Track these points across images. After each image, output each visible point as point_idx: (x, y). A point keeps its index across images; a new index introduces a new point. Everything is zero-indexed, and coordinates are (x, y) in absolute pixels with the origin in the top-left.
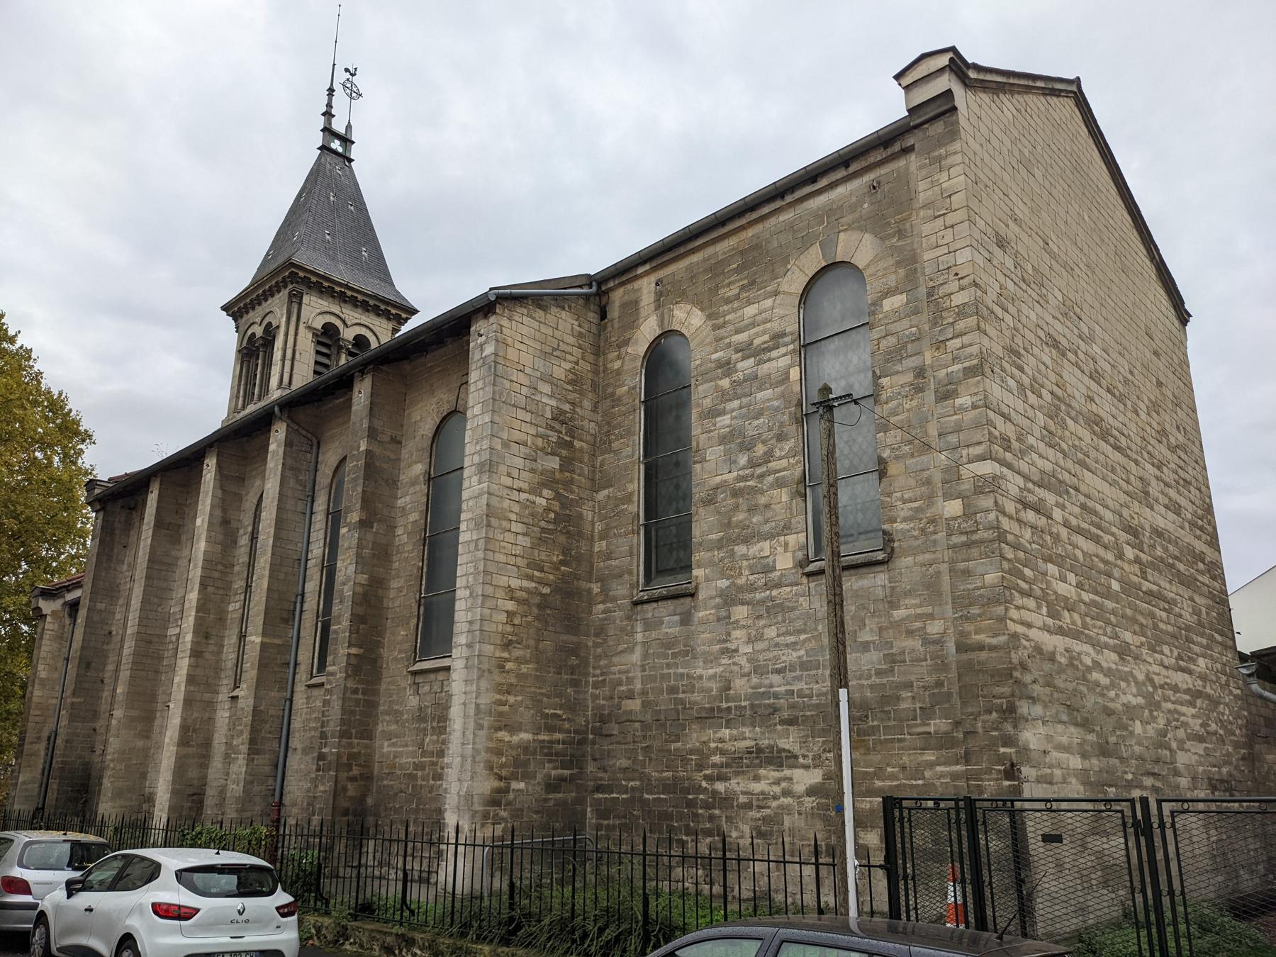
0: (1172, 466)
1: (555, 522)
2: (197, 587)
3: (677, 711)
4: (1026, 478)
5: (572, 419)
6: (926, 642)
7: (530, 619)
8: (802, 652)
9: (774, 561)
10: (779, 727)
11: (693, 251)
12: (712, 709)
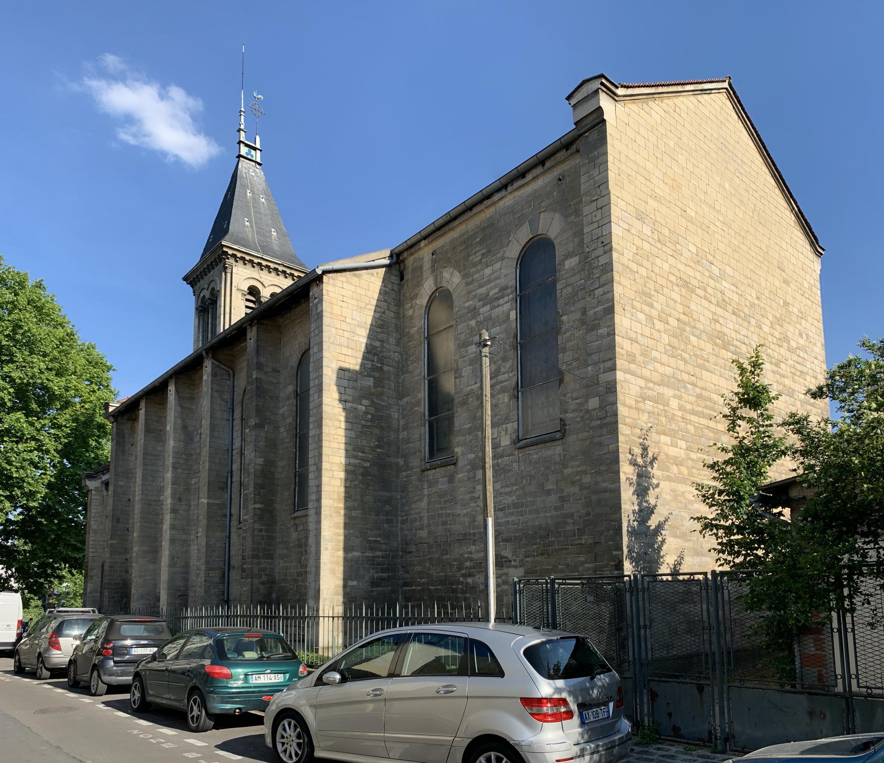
0: (791, 362)
1: (372, 420)
2: (171, 469)
3: (447, 536)
4: (647, 380)
5: (381, 352)
6: (582, 488)
7: (357, 483)
8: (514, 497)
9: (500, 441)
10: (501, 544)
11: (453, 229)
12: (465, 534)
